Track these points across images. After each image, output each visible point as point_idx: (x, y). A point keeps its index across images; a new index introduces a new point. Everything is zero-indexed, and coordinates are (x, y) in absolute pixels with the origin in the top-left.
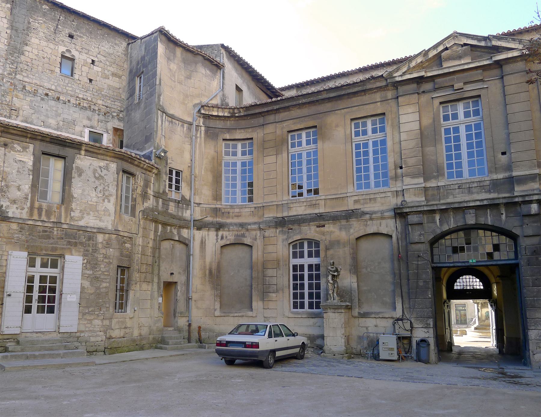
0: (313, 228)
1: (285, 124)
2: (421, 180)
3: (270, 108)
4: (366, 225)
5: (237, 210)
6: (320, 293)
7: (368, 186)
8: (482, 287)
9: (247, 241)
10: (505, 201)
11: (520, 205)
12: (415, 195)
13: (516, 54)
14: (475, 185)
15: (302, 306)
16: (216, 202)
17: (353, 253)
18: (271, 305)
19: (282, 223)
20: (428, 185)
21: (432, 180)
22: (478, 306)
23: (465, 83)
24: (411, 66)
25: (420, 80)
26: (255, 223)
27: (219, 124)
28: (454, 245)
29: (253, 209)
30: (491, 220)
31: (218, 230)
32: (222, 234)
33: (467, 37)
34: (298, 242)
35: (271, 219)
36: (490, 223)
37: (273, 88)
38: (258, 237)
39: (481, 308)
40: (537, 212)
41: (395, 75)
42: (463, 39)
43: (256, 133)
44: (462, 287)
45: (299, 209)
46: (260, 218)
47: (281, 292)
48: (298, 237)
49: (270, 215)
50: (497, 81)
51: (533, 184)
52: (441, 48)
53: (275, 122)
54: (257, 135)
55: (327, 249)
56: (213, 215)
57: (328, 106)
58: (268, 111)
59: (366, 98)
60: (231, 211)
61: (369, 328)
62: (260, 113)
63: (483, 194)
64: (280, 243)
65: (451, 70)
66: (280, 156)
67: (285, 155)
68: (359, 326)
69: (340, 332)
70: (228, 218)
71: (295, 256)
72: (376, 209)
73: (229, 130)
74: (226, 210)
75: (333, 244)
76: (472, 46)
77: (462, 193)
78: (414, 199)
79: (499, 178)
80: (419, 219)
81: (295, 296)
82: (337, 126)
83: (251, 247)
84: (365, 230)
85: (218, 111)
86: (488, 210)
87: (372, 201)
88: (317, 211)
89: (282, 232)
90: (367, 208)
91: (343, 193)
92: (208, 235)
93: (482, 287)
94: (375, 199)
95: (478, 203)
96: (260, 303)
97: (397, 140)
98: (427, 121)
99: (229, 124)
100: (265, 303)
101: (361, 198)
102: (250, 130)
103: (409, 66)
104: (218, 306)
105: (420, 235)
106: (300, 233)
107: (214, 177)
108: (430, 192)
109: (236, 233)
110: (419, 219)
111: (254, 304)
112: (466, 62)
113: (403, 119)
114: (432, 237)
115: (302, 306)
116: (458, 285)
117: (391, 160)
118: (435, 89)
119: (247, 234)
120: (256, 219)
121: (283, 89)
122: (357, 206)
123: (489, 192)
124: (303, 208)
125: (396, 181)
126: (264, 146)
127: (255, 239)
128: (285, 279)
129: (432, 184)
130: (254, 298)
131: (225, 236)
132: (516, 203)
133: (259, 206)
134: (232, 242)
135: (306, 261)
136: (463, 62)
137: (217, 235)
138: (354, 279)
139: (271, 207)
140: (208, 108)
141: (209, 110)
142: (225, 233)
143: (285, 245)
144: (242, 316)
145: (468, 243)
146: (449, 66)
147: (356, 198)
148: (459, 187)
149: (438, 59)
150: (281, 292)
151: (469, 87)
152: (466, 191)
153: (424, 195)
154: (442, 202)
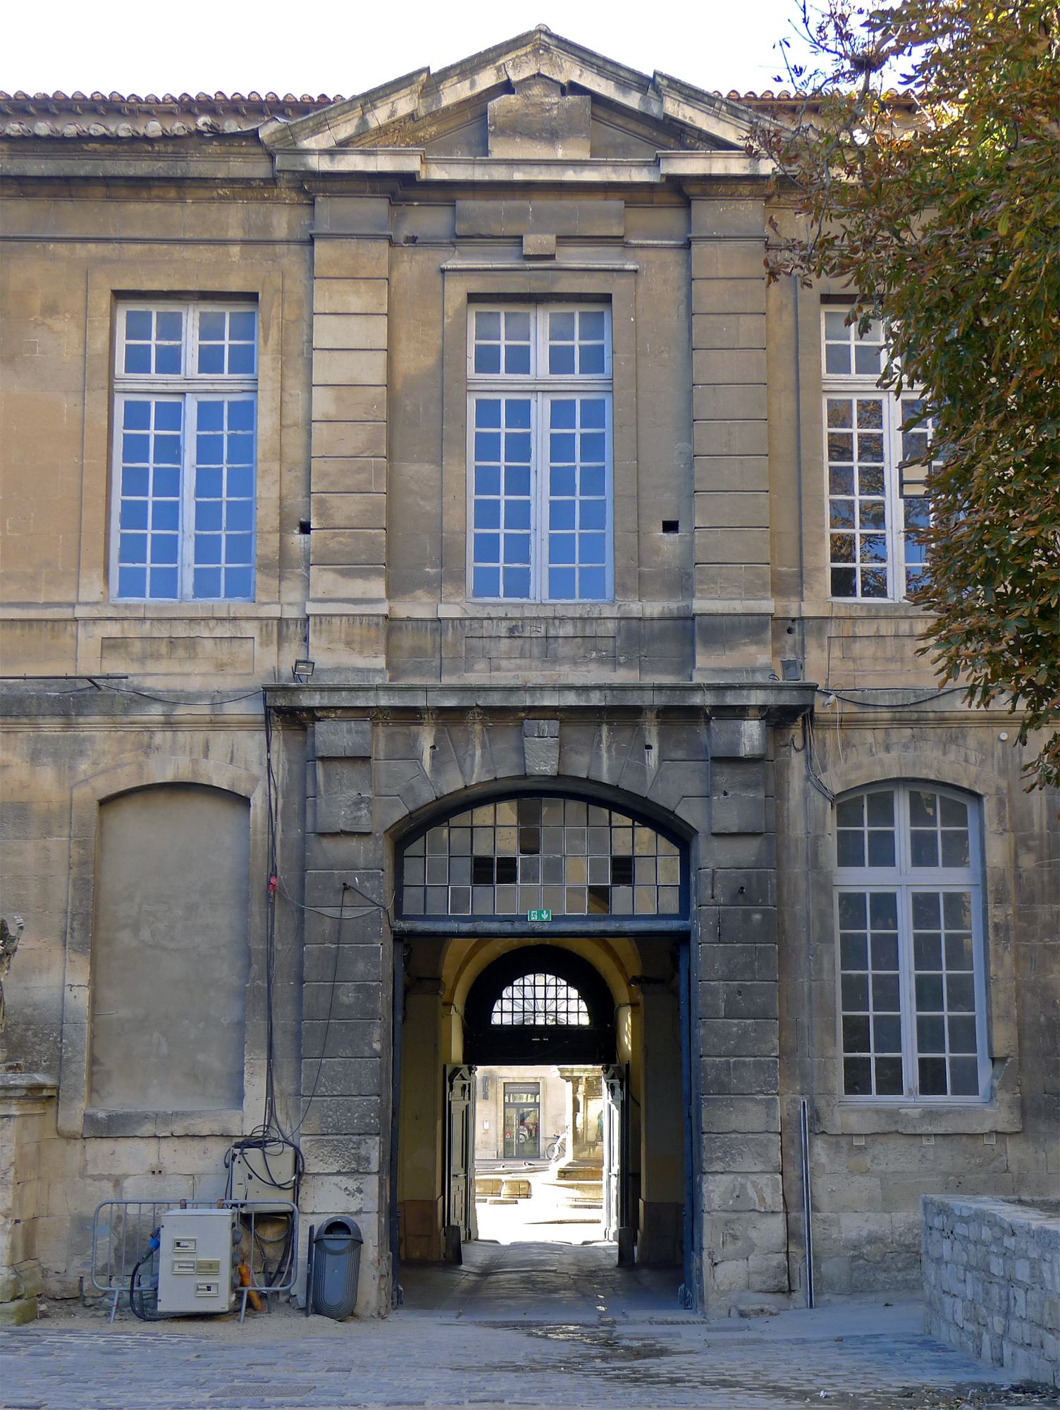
2: (377, 588)
7: (166, 584)
8: (585, 1020)
10: (660, 700)
12: (349, 643)
13: (737, 166)
14: (568, 630)
20: (404, 609)
21: (419, 593)
22: (575, 1091)
23: (563, 239)
24: (373, 124)
25: (401, 188)
30: (610, 768)
33: (583, 61)
36: (606, 779)
39: (586, 1098)
42: (567, 65)
44: (518, 1019)
51: (753, 649)
52: (487, 79)
59: (184, 215)
61: (127, 1184)
63: (593, 666)
65: (519, 176)
68: (83, 1173)
76: (597, 99)
78: (344, 660)
79: (648, 613)
82: (51, 309)
84: (140, 766)
86: (605, 728)
87: (181, 652)
90: (159, 676)
93: (585, 1020)
94: (191, 644)
95: (571, 699)
97: (296, 412)
101: (132, 631)
103: (363, 121)
105: (357, 804)
108: (407, 641)
112: (571, 159)
113: (326, 332)
116: (504, 1014)
118: (458, 240)
122: (115, 666)
123: (614, 662)
125: (281, 578)
129: (417, 607)
146: (514, 158)
147: (113, 630)
148: (511, 630)
151: (573, 257)
152: (536, 651)
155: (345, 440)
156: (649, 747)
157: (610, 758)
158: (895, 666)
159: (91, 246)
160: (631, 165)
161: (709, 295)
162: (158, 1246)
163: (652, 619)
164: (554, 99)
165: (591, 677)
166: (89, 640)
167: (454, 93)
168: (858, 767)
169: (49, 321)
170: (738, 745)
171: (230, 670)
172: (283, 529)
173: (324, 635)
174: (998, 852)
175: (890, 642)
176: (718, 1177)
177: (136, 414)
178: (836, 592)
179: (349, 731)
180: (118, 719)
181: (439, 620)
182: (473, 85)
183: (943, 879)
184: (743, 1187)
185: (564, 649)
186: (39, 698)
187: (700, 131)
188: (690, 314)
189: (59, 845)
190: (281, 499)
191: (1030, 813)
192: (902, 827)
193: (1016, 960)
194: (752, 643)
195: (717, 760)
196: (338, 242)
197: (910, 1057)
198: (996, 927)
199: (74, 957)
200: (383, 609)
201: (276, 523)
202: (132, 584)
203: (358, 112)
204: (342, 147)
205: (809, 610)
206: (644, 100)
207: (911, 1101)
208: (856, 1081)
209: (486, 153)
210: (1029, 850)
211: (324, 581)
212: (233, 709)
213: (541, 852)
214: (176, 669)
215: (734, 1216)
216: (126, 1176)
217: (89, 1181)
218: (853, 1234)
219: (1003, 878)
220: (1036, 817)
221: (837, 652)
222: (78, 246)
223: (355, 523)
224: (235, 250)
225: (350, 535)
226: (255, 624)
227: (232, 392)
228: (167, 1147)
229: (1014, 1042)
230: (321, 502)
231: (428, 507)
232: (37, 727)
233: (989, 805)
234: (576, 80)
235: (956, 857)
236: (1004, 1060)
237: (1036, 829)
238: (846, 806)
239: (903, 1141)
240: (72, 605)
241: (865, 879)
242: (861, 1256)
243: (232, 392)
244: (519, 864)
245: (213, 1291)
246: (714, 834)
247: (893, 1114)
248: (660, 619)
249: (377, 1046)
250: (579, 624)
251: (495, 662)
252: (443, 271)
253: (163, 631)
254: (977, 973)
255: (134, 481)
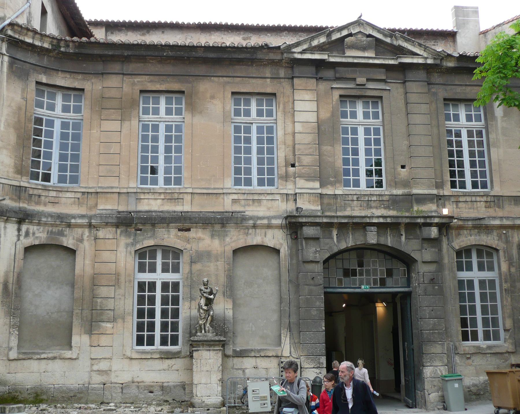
0: (174, 232)
1: (137, 79)
2: (317, 185)
3: (117, 52)
4: (247, 234)
5: (53, 194)
6: (177, 323)
7: (248, 182)
9: (68, 242)
10: (408, 221)
11: (420, 227)
12: (309, 202)
13: (421, 61)
14: (374, 198)
15: (151, 341)
16: (19, 176)
17: (229, 270)
18: (104, 340)
19: (126, 222)
20: (325, 191)
21: (329, 186)
23: (368, 80)
24: (313, 45)
25: (319, 64)
26: (82, 216)
27: (32, 59)
28: (345, 267)
29: (79, 195)
30: (391, 241)
31: (20, 222)
32: (28, 229)
33: (373, 28)
34: (147, 249)
35: (109, 212)
36: (390, 245)
37: (81, 19)
38: (85, 237)
40: (436, 237)
41: (294, 50)
42: (368, 29)
43: (89, 83)
45: (152, 202)
46: (90, 209)
47: (120, 321)
48: (151, 242)
49: (108, 206)
50: (399, 85)
51: (431, 205)
52: (345, 33)
53: (123, 74)
54: (92, 86)
55: (192, 262)
56: (14, 197)
57: (201, 70)
58: (112, 56)
59: (253, 71)
60: (44, 193)
61: (247, 371)
62: (101, 56)
63: (382, 210)
64: (122, 248)
65: (356, 61)
66: (126, 124)
67: (135, 122)
68: (233, 368)
69: (216, 377)
70: (38, 203)
71: (142, 269)
72: (261, 214)
73: (46, 70)
74: (36, 192)
75: (199, 257)
76: (377, 40)
77: (361, 206)
78: (309, 206)
79: (398, 194)
80: (316, 232)
81: (140, 327)
82: (213, 97)
83: (72, 252)
84: (246, 240)
85: (33, 38)
86: (389, 229)
87: (256, 204)
88: (179, 208)
89: (127, 234)
90: (251, 211)
91: (218, 189)
92: (5, 228)
94: (259, 201)
95: (381, 220)
96: (85, 338)
97: (289, 129)
98: (325, 114)
99: (45, 62)
100: (94, 337)
101: (241, 197)
102: (80, 77)
103: (311, 44)
104: (14, 342)
105: (316, 252)
106: (153, 236)
107: (18, 137)
108: (326, 201)
109: (50, 229)
110: (316, 232)
111: (75, 339)
112: (369, 56)
113: (299, 105)
114: (327, 255)
115: (151, 341)
117: (281, 154)
118: (338, 79)
119: (67, 231)
120: (82, 211)
121: (97, 24)
122: (237, 208)
123: (387, 208)
124: (159, 201)
125: (286, 181)
126: (102, 105)
127: (81, 240)
128: (129, 304)
129: (329, 191)
130: (74, 331)
131: (31, 231)
132: (418, 224)
133: (90, 191)
134: (43, 241)
135: (159, 277)
136: (366, 54)
137: (19, 230)
138: (229, 305)
139: (109, 195)
140: (19, 29)
141: (20, 33)
142: (33, 228)
143: (130, 253)
144: (54, 358)
145: (361, 265)
146: (352, 55)
147: (235, 197)
148: (357, 198)
149: (339, 45)
150: (120, 321)
151: (371, 85)
152: (365, 205)
153: (319, 203)
154: (339, 214)
155: (305, 139)
156: (402, 235)
157: (390, 238)
158: (472, 210)
159: (225, 78)
160: (389, 59)
161: (413, 98)
162: (247, 392)
163: (399, 195)
164: (365, 39)
165: (378, 213)
166: (228, 200)
167: (336, 36)
168: (463, 241)
169: (212, 101)
170: (431, 234)
171: (271, 209)
172: (286, 166)
173: (302, 199)
174: (504, 267)
175: (469, 203)
176: (429, 367)
177: (237, 129)
178: (452, 187)
179: (313, 230)
180: (239, 225)
181: (335, 195)
182: (341, 34)
183: (486, 275)
184: (436, 370)
185: (373, 204)
186: (214, 218)
187: (409, 50)
188: (407, 103)
189: (221, 265)
190: (285, 156)
191: (513, 255)
192: (475, 260)
193: (511, 300)
194: (431, 203)
195: (424, 239)
196: (300, 79)
197: (480, 329)
198: (505, 290)
199: (227, 300)
200: (319, 191)
201: (284, 164)
202: (237, 182)
203: (309, 41)
204: (304, 52)
205: (446, 193)
206: (392, 40)
207: (481, 343)
208: (465, 337)
209: (344, 53)
210: (513, 266)
211: (301, 183)
212: (275, 222)
213: (364, 266)
214: (255, 209)
215: (434, 379)
216: (246, 369)
217: (235, 370)
218: (468, 384)
219: (506, 275)
220: (514, 256)
221: (455, 206)
222: (221, 78)
223: (310, 164)
224: (268, 80)
225: (308, 168)
226: (279, 195)
227: (267, 123)
228: (258, 360)
229: (512, 325)
230: (299, 158)
231: (330, 159)
232: (213, 227)
233: (501, 253)
234: (371, 33)
235: (491, 268)
236: (508, 330)
237: (515, 260)
238: (459, 253)
239: (481, 355)
240: (222, 189)
241: (464, 275)
242: (471, 391)
243: (267, 123)
244: (357, 271)
245: (266, 406)
246: (423, 262)
247: (478, 347)
248: (401, 195)
249: (324, 328)
250: (378, 197)
251: (353, 208)
252: (332, 88)
253: (251, 197)
254: (499, 303)
255: (237, 150)
